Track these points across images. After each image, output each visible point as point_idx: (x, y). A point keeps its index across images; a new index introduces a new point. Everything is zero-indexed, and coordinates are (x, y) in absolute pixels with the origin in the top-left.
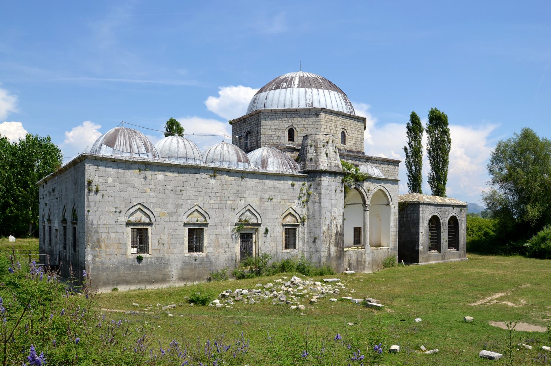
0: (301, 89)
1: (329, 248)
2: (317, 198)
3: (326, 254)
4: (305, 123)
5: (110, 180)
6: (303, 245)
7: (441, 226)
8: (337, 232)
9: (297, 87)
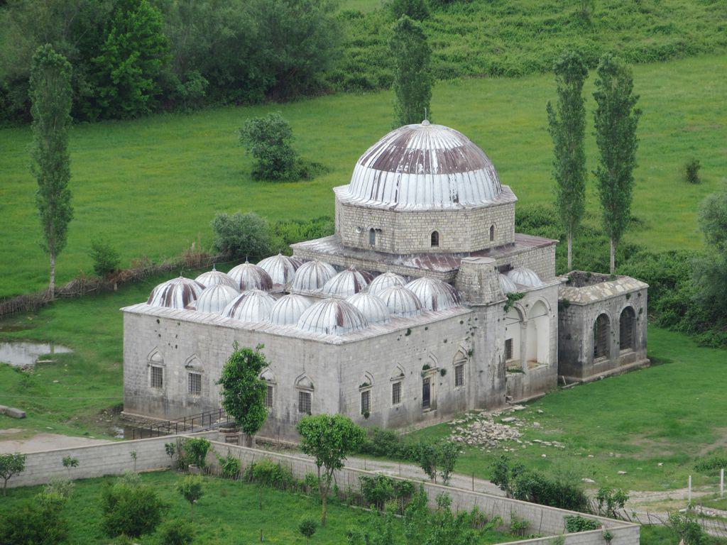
0: (442, 175)
1: (493, 381)
2: (482, 333)
3: (491, 387)
4: (452, 226)
5: (351, 358)
6: (470, 380)
7: (611, 325)
8: (500, 363)
9: (438, 173)
